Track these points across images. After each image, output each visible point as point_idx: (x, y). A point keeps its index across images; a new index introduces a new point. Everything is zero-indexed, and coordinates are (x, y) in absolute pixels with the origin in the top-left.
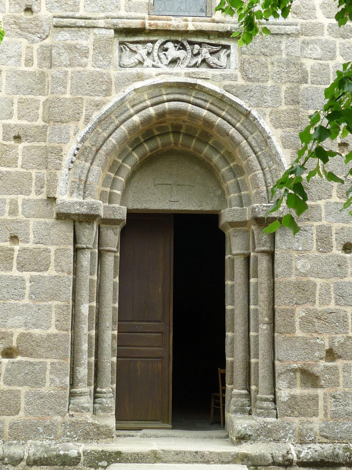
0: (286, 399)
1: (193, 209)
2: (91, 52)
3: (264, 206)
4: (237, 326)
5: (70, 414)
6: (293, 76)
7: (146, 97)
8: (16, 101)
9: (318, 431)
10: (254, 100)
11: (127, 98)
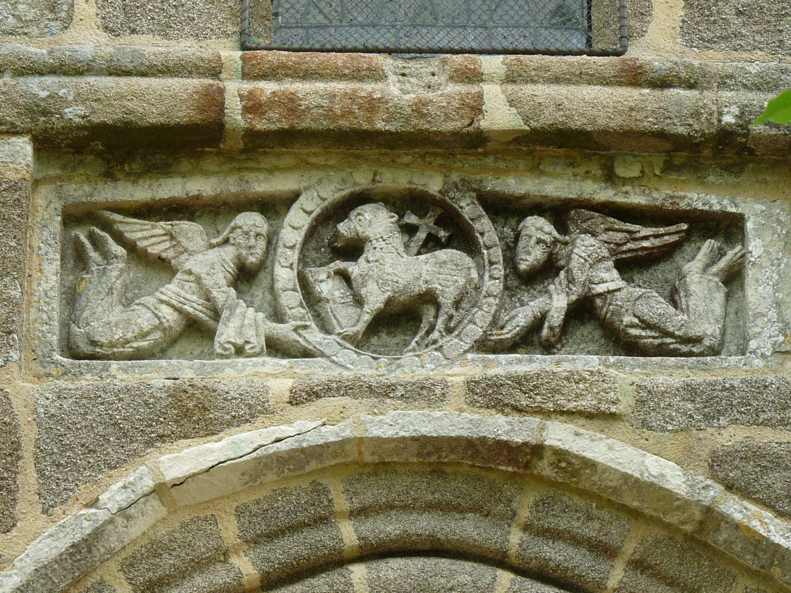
11: (113, 538)
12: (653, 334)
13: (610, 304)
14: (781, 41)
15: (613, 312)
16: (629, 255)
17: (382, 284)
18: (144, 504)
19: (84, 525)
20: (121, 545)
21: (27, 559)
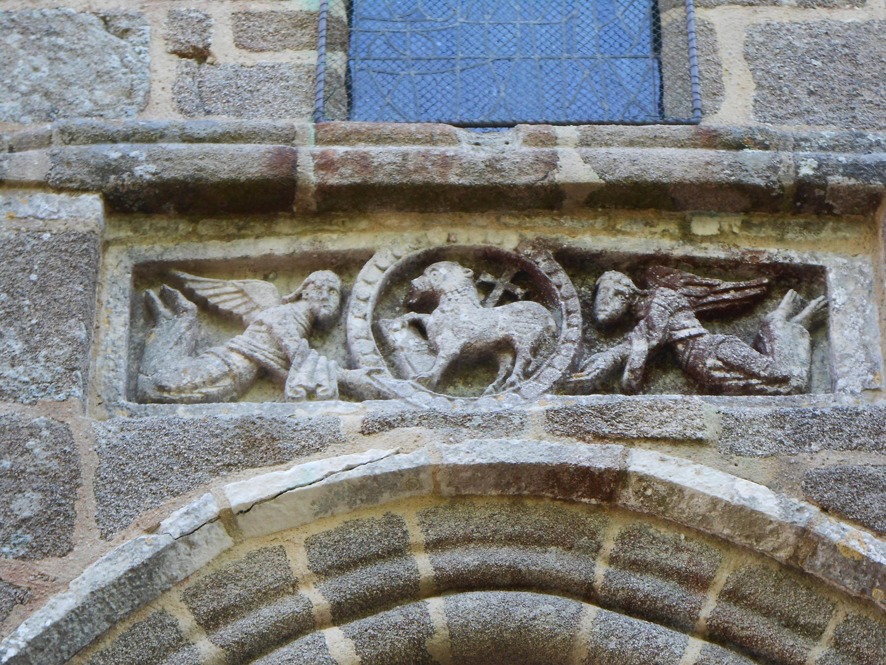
11: (176, 566)
12: (738, 375)
13: (692, 349)
14: (854, 117)
15: (695, 355)
16: (710, 307)
18: (209, 530)
19: (144, 549)
20: (184, 575)
21: (84, 582)
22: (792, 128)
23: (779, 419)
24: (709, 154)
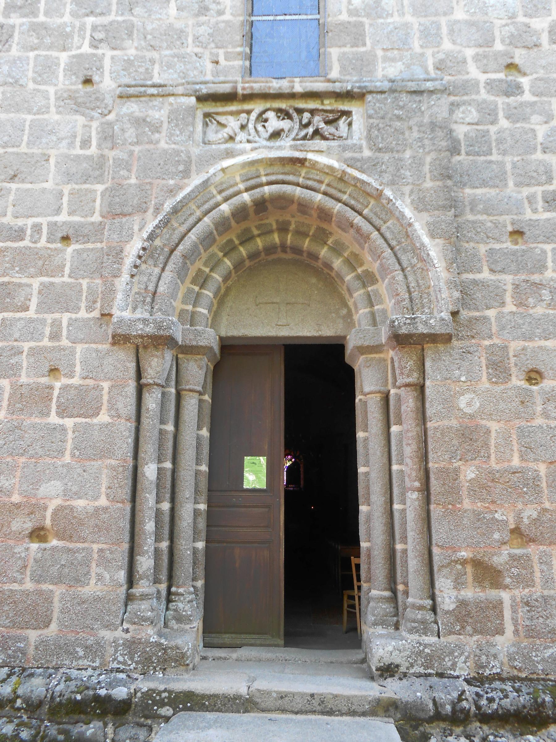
0: (452, 607)
1: (309, 334)
2: (165, 125)
3: (407, 318)
4: (374, 496)
5: (123, 629)
6: (440, 143)
7: (238, 179)
8: (66, 192)
9: (505, 660)
10: (387, 177)
17: (272, 127)
22: (348, 78)
23: (340, 146)
24: (327, 84)
